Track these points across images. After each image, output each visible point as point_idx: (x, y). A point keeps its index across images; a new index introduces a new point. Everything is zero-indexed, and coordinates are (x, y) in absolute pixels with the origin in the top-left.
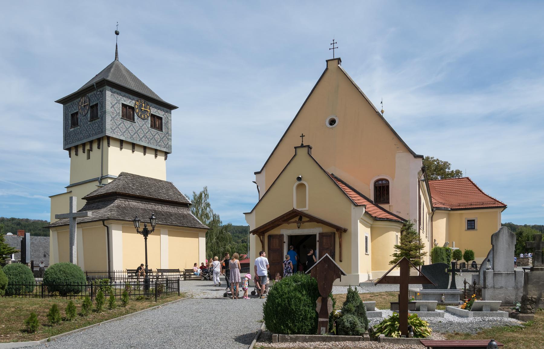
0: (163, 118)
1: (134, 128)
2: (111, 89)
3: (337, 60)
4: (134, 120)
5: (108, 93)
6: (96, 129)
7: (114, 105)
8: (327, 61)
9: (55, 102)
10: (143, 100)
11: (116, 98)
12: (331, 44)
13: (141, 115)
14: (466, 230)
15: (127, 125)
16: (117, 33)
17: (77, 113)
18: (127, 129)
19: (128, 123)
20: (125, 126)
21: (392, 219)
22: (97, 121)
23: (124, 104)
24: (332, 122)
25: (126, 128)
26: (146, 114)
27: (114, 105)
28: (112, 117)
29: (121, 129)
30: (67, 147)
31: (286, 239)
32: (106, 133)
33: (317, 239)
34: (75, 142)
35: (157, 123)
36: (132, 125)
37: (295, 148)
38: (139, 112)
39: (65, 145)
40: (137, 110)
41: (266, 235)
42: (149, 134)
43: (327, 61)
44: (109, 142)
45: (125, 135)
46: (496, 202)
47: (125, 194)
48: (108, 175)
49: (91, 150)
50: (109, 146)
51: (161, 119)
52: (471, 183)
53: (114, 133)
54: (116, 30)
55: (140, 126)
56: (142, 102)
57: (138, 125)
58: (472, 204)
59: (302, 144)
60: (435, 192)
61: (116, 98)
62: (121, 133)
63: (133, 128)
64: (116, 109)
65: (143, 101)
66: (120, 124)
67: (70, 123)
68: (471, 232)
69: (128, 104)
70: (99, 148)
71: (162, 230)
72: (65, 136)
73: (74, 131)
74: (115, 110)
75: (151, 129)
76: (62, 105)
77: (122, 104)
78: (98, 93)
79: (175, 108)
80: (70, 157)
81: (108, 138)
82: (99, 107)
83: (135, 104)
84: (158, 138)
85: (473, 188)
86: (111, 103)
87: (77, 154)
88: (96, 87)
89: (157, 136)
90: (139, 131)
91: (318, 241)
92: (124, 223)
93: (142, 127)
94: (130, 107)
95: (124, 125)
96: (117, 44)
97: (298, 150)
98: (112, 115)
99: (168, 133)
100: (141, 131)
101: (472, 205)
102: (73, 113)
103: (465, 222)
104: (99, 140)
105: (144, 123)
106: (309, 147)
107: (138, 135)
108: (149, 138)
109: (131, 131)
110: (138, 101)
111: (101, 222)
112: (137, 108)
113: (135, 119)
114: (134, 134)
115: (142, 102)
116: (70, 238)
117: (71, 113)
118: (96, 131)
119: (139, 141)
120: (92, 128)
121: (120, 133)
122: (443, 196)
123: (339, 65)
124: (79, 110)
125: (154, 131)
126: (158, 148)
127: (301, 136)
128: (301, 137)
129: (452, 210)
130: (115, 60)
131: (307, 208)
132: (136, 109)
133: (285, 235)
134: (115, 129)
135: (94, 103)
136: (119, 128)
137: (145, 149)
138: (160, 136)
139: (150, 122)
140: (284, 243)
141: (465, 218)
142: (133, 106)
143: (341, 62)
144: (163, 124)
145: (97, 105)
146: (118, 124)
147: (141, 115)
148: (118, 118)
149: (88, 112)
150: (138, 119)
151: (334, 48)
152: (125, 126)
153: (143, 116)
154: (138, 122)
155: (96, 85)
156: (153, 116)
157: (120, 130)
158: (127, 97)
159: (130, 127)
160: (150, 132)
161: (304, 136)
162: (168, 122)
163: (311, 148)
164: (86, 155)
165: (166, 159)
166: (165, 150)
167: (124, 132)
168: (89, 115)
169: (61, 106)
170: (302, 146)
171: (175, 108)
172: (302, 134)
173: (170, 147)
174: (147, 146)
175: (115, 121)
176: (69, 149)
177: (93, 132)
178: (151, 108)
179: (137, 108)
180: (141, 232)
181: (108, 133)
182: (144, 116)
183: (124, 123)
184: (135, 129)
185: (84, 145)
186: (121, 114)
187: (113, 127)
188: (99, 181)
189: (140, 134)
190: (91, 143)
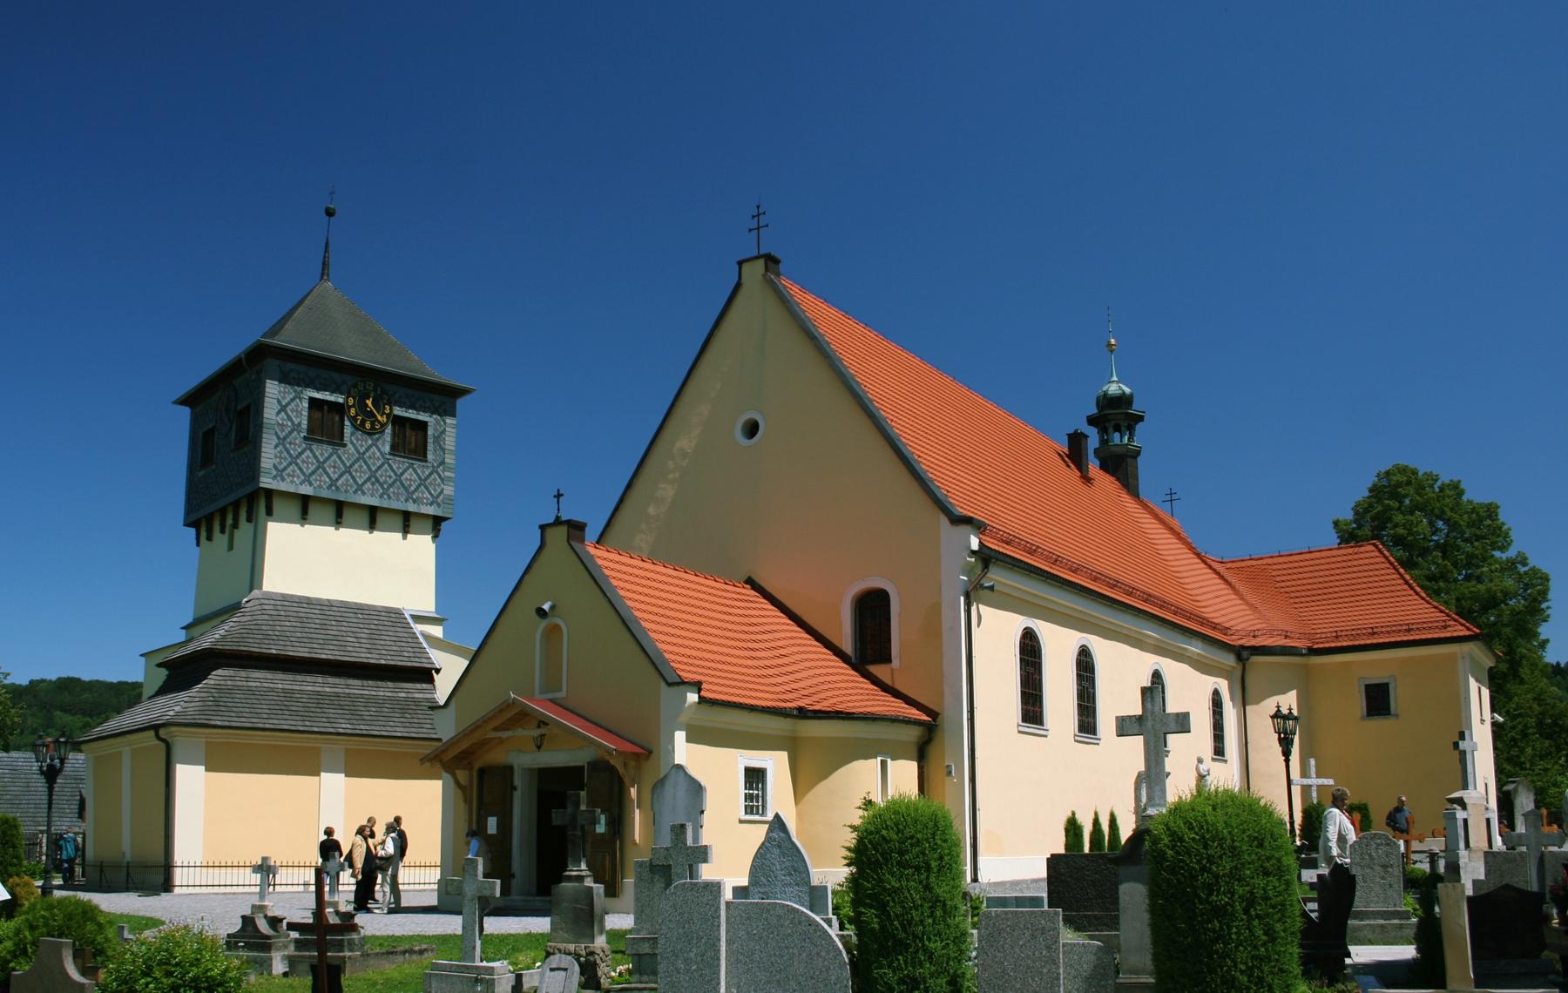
0: (429, 424)
14: (1362, 718)
15: (322, 455)
16: (330, 213)
17: (212, 431)
18: (321, 465)
19: (322, 451)
21: (854, 713)
24: (752, 429)
25: (318, 461)
28: (278, 437)
29: (304, 466)
30: (194, 517)
32: (259, 482)
36: (335, 452)
38: (357, 414)
40: (353, 411)
44: (272, 503)
45: (313, 482)
46: (1448, 623)
49: (235, 525)
53: (283, 479)
55: (358, 452)
58: (1375, 630)
59: (558, 518)
60: (1273, 593)
62: (303, 478)
66: (300, 454)
67: (199, 455)
74: (289, 418)
80: (198, 545)
81: (269, 494)
86: (279, 402)
89: (411, 475)
93: (364, 453)
96: (327, 239)
97: (549, 531)
101: (1374, 633)
105: (370, 442)
107: (353, 478)
108: (385, 482)
109: (332, 469)
111: (151, 733)
112: (353, 406)
119: (355, 492)
121: (298, 477)
122: (1296, 606)
125: (399, 464)
126: (411, 507)
129: (1313, 652)
133: (516, 768)
134: (285, 468)
136: (297, 464)
138: (418, 475)
144: (430, 440)
150: (352, 434)
153: (368, 426)
154: (355, 442)
156: (398, 422)
160: (390, 466)
164: (226, 538)
166: (431, 510)
168: (233, 436)
169: (185, 412)
170: (558, 522)
172: (558, 490)
175: (288, 446)
179: (353, 406)
181: (266, 482)
183: (311, 451)
184: (343, 462)
190: (236, 506)
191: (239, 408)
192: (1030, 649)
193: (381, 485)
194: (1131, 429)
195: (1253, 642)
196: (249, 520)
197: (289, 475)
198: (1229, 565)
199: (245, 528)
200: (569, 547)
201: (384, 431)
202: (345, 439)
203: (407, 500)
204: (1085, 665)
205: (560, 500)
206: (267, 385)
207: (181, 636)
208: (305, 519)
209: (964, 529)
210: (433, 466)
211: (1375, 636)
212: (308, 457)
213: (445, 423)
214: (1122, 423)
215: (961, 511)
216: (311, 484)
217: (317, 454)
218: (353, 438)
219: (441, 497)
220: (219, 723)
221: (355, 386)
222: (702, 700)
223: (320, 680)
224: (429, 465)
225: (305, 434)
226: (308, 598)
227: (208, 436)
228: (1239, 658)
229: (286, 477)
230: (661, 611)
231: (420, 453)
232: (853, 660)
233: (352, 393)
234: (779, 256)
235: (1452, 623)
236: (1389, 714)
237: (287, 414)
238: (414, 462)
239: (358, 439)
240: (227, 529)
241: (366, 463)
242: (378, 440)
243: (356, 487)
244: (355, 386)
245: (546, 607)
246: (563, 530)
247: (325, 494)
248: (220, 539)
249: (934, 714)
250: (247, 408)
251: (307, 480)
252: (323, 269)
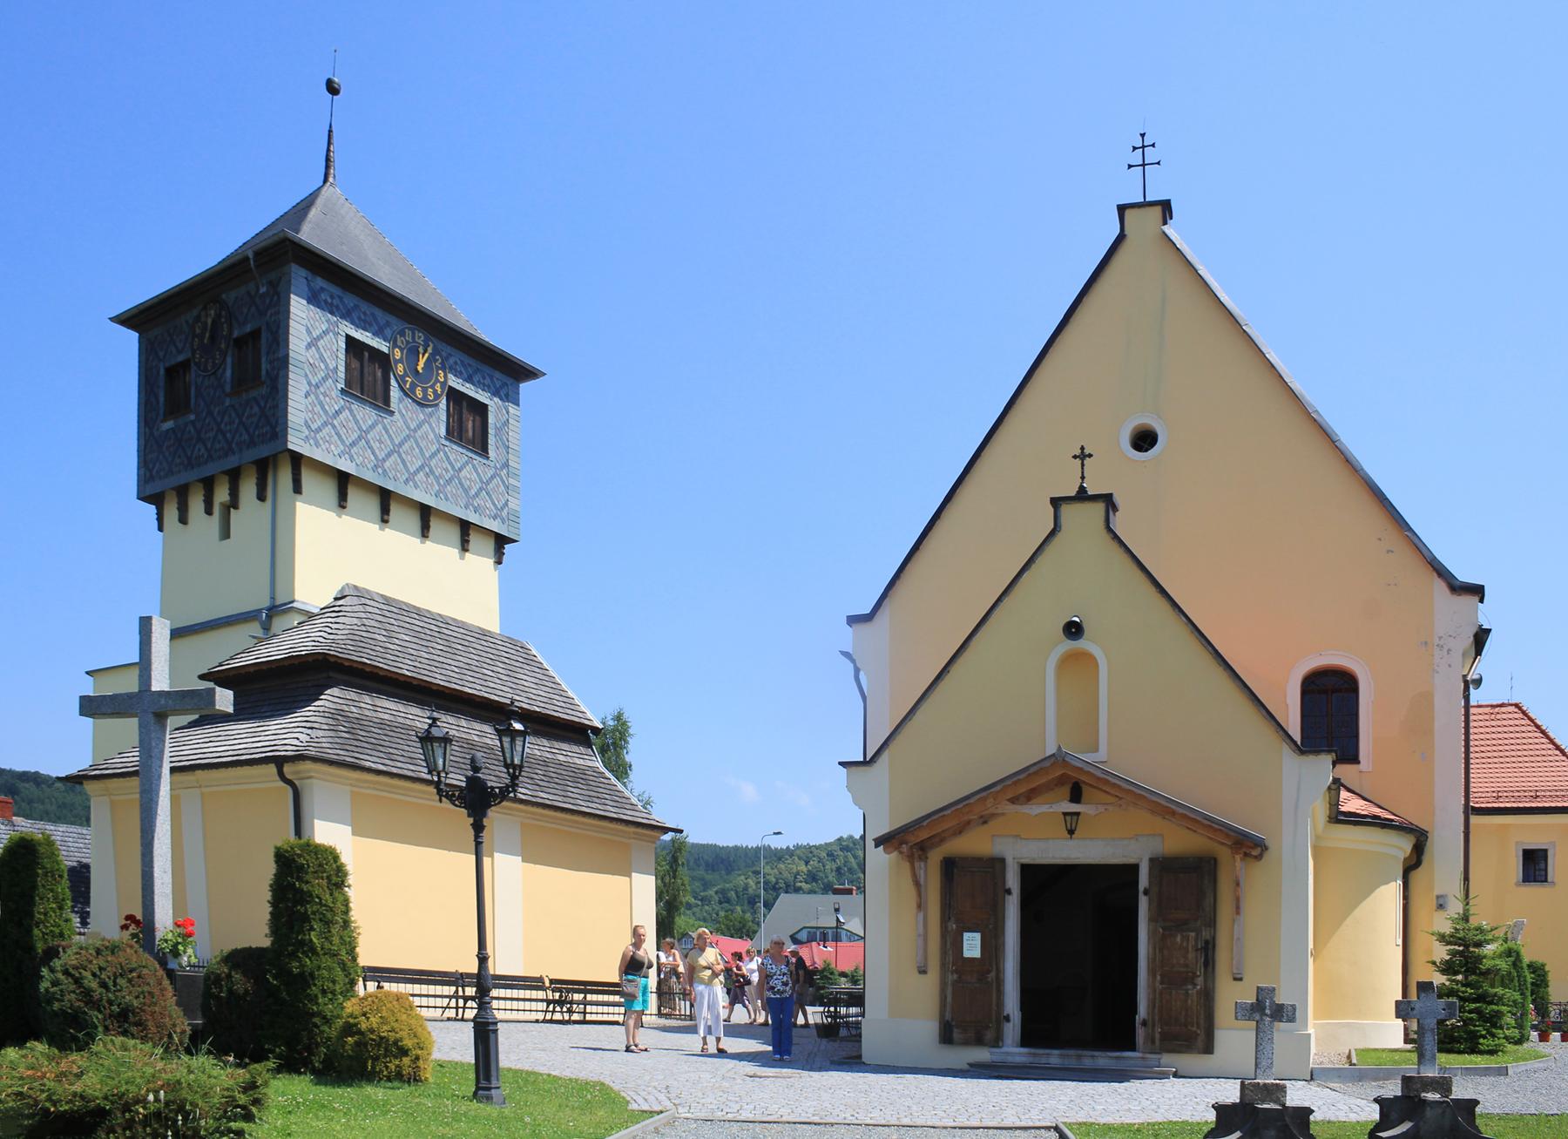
0: (490, 408)
1: (387, 432)
3: (1158, 209)
4: (387, 401)
5: (301, 314)
6: (252, 423)
7: (319, 338)
8: (1122, 209)
9: (114, 319)
10: (419, 331)
12: (1135, 148)
13: (413, 386)
14: (1517, 884)
16: (332, 89)
17: (185, 365)
19: (366, 414)
20: (357, 422)
22: (254, 393)
23: (354, 338)
25: (360, 428)
26: (431, 387)
27: (319, 338)
28: (309, 383)
29: (342, 431)
30: (149, 491)
31: (1013, 880)
33: (1144, 881)
34: (179, 472)
35: (470, 425)
37: (1056, 502)
38: (406, 375)
40: (400, 368)
41: (936, 857)
42: (441, 460)
43: (1122, 209)
45: (355, 457)
47: (360, 667)
48: (292, 602)
49: (234, 503)
52: (1530, 723)
53: (317, 445)
54: (335, 97)
56: (420, 337)
57: (400, 423)
58: (1500, 794)
59: (1082, 489)
63: (383, 432)
64: (325, 355)
65: (420, 337)
66: (337, 413)
67: (162, 399)
68: (1534, 890)
70: (261, 497)
72: (143, 447)
74: (323, 359)
75: (447, 443)
76: (137, 334)
78: (263, 290)
80: (161, 529)
81: (297, 460)
82: (263, 341)
84: (470, 480)
86: (309, 332)
87: (183, 520)
88: (257, 267)
90: (406, 446)
91: (1146, 892)
92: (357, 780)
93: (415, 431)
95: (354, 416)
96: (330, 126)
97: (1066, 510)
98: (310, 376)
99: (506, 465)
100: (412, 448)
102: (173, 362)
103: (1517, 856)
104: (264, 469)
106: (1108, 501)
107: (403, 462)
108: (441, 476)
111: (272, 769)
112: (401, 361)
113: (392, 399)
114: (389, 455)
115: (420, 337)
116: (141, 805)
117: (167, 365)
118: (251, 430)
119: (406, 482)
120: (237, 421)
123: (1165, 228)
124: (194, 353)
125: (458, 454)
126: (472, 518)
127: (1075, 457)
128: (1078, 461)
130: (326, 180)
132: (397, 362)
134: (319, 430)
135: (248, 328)
136: (334, 427)
139: (444, 419)
140: (1007, 897)
141: (1517, 843)
143: (1171, 218)
144: (491, 431)
146: (331, 411)
147: (413, 386)
148: (330, 389)
149: (224, 361)
150: (401, 401)
151: (1144, 165)
152: (357, 422)
153: (419, 392)
154: (404, 412)
155: (254, 261)
156: (454, 396)
157: (338, 434)
159: (372, 427)
161: (1090, 456)
163: (1115, 509)
166: (495, 526)
167: (353, 444)
168: (228, 373)
169: (132, 337)
170: (1082, 496)
172: (1082, 448)
175: (321, 397)
176: (156, 499)
177: (241, 435)
180: (453, 795)
181: (295, 443)
182: (425, 390)
183: (351, 411)
186: (342, 375)
187: (314, 421)
188: (261, 624)
189: (408, 458)
190: (234, 477)
191: (236, 334)
193: (437, 479)
199: (250, 513)
200: (1107, 537)
201: (437, 405)
202: (392, 405)
205: (1085, 462)
206: (292, 302)
208: (344, 507)
210: (496, 468)
211: (1538, 800)
212: (347, 420)
213: (508, 413)
215: (1464, 575)
217: (358, 417)
218: (401, 405)
219: (505, 511)
220: (368, 764)
221: (402, 334)
223: (463, 723)
224: (492, 464)
225: (343, 386)
226: (418, 609)
227: (175, 373)
229: (321, 442)
233: (399, 343)
236: (1546, 881)
238: (474, 456)
239: (407, 409)
240: (217, 509)
242: (431, 415)
243: (407, 475)
244: (402, 334)
250: (255, 335)
251: (347, 452)
252: (327, 167)
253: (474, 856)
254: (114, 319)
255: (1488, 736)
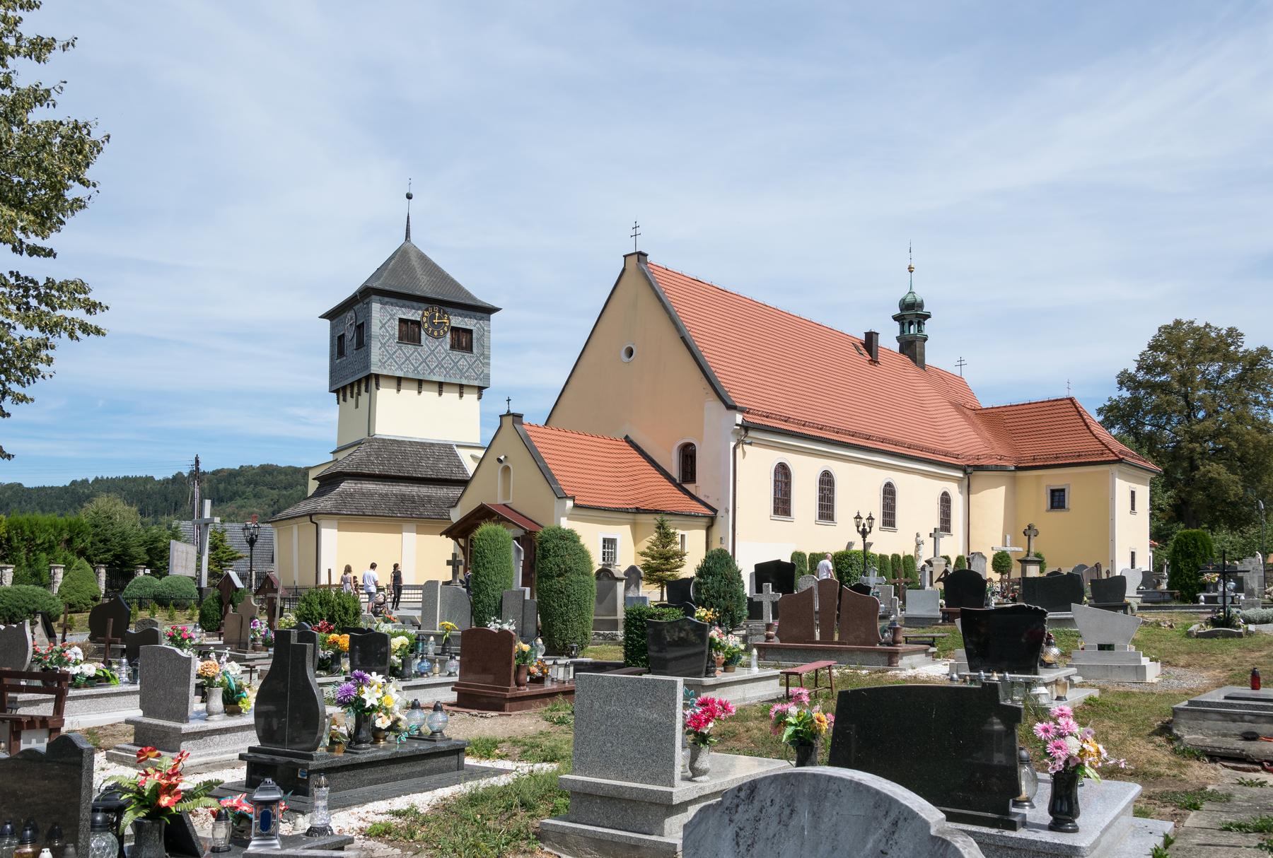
2: (381, 298)
9: (321, 317)
11: (388, 312)
13: (433, 331)
14: (1047, 511)
15: (408, 352)
16: (409, 197)
17: (343, 335)
18: (407, 359)
19: (409, 349)
28: (381, 343)
29: (397, 360)
30: (335, 387)
37: (501, 416)
38: (429, 327)
39: (331, 384)
40: (426, 325)
43: (625, 256)
49: (359, 394)
50: (378, 389)
51: (470, 332)
53: (385, 368)
57: (426, 349)
59: (508, 411)
61: (388, 312)
68: (1058, 515)
69: (411, 318)
71: (405, 526)
73: (340, 363)
74: (387, 331)
77: (400, 319)
79: (496, 310)
81: (377, 376)
83: (423, 315)
85: (1075, 421)
86: (380, 321)
94: (414, 322)
97: (504, 418)
99: (483, 354)
101: (1057, 457)
107: (428, 366)
110: (427, 310)
111: (308, 518)
119: (429, 374)
125: (456, 355)
126: (464, 382)
129: (1018, 469)
131: (510, 501)
136: (393, 359)
137: (441, 386)
142: (419, 319)
144: (474, 341)
145: (363, 323)
147: (433, 331)
150: (426, 339)
153: (436, 334)
156: (455, 330)
157: (395, 362)
158: (408, 307)
162: (484, 333)
165: (479, 398)
166: (476, 383)
169: (327, 322)
170: (509, 414)
171: (496, 310)
173: (487, 377)
174: (443, 380)
176: (337, 391)
178: (451, 317)
179: (426, 322)
181: (375, 369)
182: (439, 332)
183: (401, 350)
185: (352, 385)
186: (397, 336)
192: (783, 475)
193: (445, 369)
194: (919, 324)
195: (977, 463)
196: (367, 391)
197: (388, 365)
198: (978, 412)
199: (364, 397)
203: (461, 378)
204: (827, 482)
207: (331, 458)
209: (733, 412)
214: (914, 320)
216: (402, 370)
222: (576, 506)
228: (965, 471)
230: (557, 457)
231: (469, 348)
232: (678, 481)
234: (644, 251)
235: (1107, 451)
237: (386, 329)
240: (355, 395)
241: (435, 356)
242: (442, 341)
245: (502, 458)
246: (511, 417)
247: (410, 376)
248: (351, 401)
249: (715, 511)
253: (704, 532)
254: (321, 317)
255: (1051, 420)
